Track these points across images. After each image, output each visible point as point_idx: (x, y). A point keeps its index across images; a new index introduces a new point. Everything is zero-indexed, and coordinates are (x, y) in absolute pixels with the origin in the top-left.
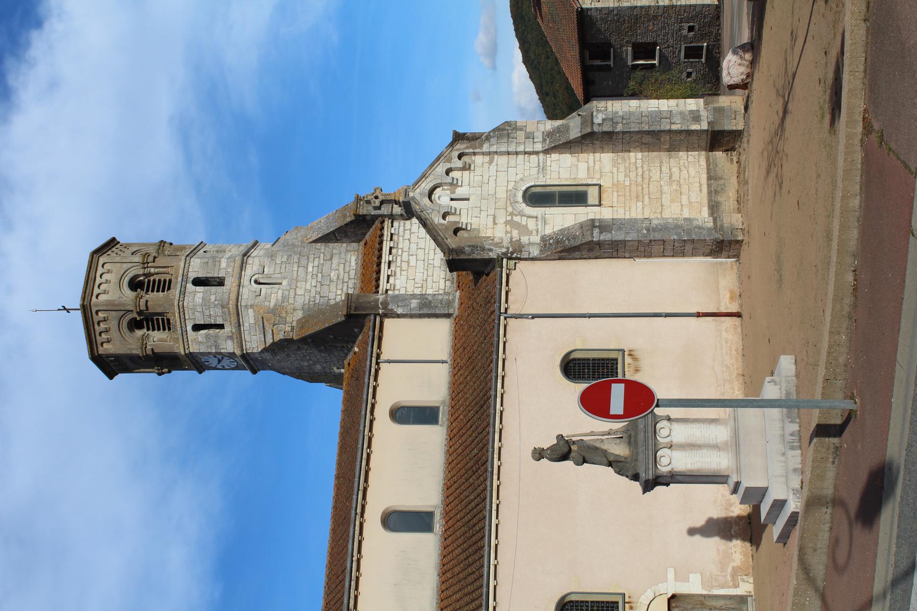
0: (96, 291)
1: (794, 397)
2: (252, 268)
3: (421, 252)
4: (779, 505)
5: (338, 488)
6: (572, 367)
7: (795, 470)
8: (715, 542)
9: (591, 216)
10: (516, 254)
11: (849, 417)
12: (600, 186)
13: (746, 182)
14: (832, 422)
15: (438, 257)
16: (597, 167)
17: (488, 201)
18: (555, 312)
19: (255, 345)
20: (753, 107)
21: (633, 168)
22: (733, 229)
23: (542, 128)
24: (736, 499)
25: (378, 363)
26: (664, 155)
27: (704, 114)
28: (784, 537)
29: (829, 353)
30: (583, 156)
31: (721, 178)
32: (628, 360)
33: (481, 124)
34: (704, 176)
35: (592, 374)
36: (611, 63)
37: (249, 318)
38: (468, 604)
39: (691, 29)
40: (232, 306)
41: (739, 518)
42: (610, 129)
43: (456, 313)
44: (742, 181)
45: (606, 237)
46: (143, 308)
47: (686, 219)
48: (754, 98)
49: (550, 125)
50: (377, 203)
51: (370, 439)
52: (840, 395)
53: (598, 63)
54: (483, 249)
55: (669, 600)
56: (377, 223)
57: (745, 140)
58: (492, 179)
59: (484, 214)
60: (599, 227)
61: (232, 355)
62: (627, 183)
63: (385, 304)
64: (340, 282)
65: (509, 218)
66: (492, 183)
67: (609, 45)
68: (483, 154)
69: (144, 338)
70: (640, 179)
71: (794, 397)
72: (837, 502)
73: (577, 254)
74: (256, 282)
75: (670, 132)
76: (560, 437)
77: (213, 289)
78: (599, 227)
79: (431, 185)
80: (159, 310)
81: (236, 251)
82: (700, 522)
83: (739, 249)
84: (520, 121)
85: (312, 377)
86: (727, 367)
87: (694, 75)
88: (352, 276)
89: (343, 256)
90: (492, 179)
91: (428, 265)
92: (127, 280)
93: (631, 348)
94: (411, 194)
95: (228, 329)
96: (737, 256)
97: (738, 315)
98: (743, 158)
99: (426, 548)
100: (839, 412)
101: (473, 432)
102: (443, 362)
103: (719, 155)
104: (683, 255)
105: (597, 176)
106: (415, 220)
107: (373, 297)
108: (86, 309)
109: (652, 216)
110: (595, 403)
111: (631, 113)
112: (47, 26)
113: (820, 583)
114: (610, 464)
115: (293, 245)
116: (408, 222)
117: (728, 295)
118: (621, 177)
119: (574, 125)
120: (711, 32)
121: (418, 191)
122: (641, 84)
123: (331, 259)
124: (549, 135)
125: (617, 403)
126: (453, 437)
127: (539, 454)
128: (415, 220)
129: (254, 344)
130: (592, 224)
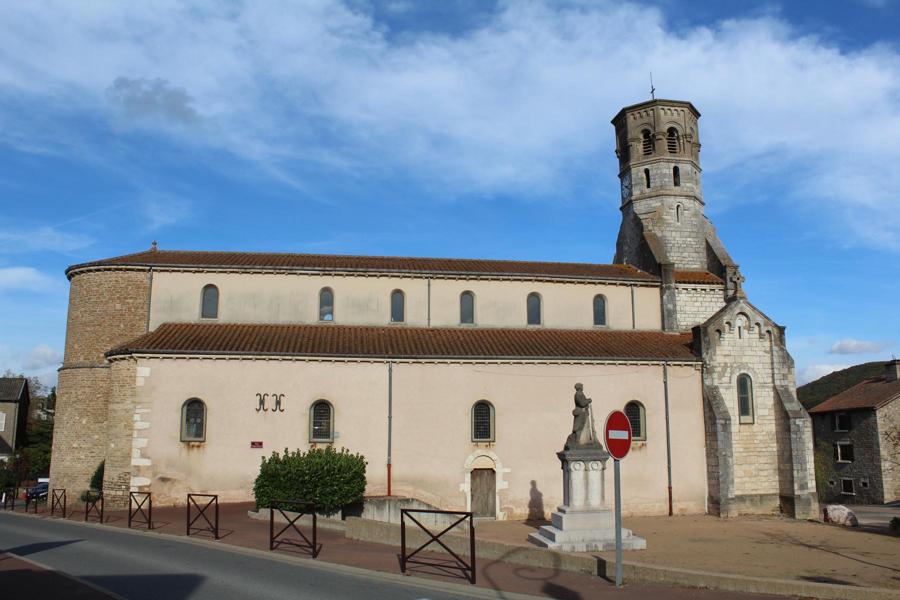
0: (666, 108)
1: (623, 548)
2: (686, 202)
4: (552, 537)
5: (552, 265)
6: (634, 407)
7: (573, 547)
8: (527, 497)
11: (611, 581)
12: (753, 424)
13: (759, 520)
14: (607, 570)
15: (701, 320)
16: (765, 422)
17: (739, 350)
18: (671, 395)
20: (812, 525)
21: (766, 445)
22: (727, 511)
23: (791, 384)
24: (555, 510)
25: (631, 285)
26: (776, 465)
27: (806, 492)
28: (532, 540)
31: (761, 503)
32: (640, 443)
33: (791, 345)
34: (762, 492)
35: (630, 418)
36: (838, 431)
37: (655, 203)
39: (865, 484)
40: (662, 192)
41: (543, 513)
44: (760, 517)
46: (657, 137)
48: (819, 526)
49: (793, 390)
50: (734, 280)
51: (583, 283)
52: (625, 576)
53: (837, 422)
54: (708, 349)
55: (492, 469)
56: (721, 280)
57: (789, 519)
58: (754, 353)
59: (731, 348)
61: (631, 194)
63: (669, 288)
67: (850, 429)
68: (771, 347)
70: (759, 450)
71: (623, 548)
72: (557, 572)
74: (678, 206)
75: (792, 470)
76: (590, 401)
80: (656, 147)
81: (697, 192)
82: (540, 488)
83: (714, 515)
84: (796, 369)
85: (619, 245)
87: (832, 486)
90: (754, 353)
91: (695, 314)
92: (674, 126)
95: (647, 190)
96: (709, 513)
97: (671, 513)
98: (776, 518)
99: (311, 316)
100: (614, 575)
102: (634, 326)
103: (777, 502)
104: (709, 478)
105: (760, 422)
106: (724, 304)
107: (673, 280)
108: (654, 102)
109: (734, 458)
110: (615, 421)
111: (804, 443)
112: (843, 57)
113: (507, 560)
114: (574, 432)
115: (703, 228)
119: (793, 406)
122: (824, 450)
124: (786, 389)
125: (616, 435)
126: (587, 334)
127: (579, 388)
128: (724, 304)
129: (639, 208)
130: (728, 419)
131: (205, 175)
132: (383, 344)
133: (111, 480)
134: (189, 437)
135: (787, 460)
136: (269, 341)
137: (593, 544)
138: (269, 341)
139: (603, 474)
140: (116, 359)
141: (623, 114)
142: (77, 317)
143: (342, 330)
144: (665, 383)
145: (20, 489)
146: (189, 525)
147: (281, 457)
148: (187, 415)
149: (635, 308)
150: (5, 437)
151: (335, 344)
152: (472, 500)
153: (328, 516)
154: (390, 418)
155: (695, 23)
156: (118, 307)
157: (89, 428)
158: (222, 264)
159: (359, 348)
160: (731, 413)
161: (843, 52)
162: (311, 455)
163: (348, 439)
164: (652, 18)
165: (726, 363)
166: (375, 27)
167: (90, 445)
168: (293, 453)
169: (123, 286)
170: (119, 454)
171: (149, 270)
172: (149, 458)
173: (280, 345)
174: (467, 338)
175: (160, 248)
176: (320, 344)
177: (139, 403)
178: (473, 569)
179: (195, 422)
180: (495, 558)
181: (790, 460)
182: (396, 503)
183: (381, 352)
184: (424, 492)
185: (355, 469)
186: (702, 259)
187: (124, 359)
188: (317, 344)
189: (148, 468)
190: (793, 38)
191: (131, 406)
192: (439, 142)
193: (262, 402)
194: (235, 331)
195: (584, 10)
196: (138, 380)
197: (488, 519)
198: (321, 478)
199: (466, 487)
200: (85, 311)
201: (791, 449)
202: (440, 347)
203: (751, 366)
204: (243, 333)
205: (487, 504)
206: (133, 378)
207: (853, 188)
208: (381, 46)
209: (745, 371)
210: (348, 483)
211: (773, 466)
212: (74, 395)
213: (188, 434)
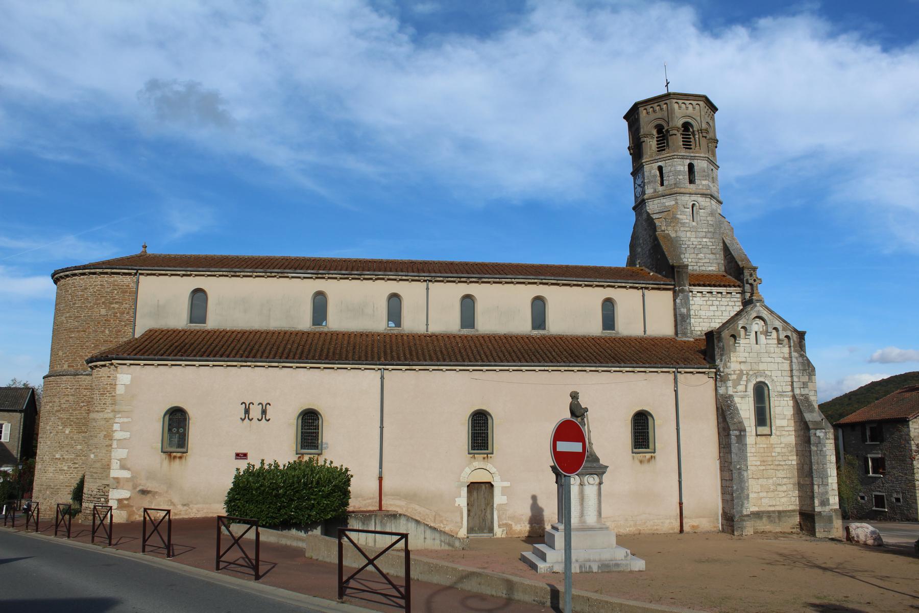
3: (719, 313)
4: (543, 557)
5: (560, 267)
8: (527, 513)
9: (747, 429)
12: (771, 435)
13: (776, 538)
15: (716, 325)
16: (784, 433)
17: (756, 356)
18: (684, 403)
20: (832, 545)
22: (742, 528)
23: (812, 393)
25: (642, 288)
26: (795, 480)
27: (827, 509)
29: (607, 602)
30: (792, 423)
31: (780, 520)
32: (648, 456)
33: (811, 353)
34: (781, 509)
36: (868, 443)
37: (669, 202)
38: (485, 353)
39: (898, 500)
42: (812, 442)
43: (678, 339)
44: (777, 536)
45: (733, 439)
46: (671, 133)
47: (748, 495)
48: (839, 546)
50: (750, 281)
51: (591, 286)
53: (868, 433)
54: (722, 355)
56: (739, 283)
57: (808, 538)
58: (772, 360)
59: (747, 355)
61: (643, 193)
62: (773, 454)
63: (682, 291)
66: (769, 360)
67: (882, 441)
68: (790, 353)
69: (651, 135)
70: (777, 463)
73: (721, 420)
74: (693, 205)
75: (812, 484)
76: (586, 410)
77: (687, 177)
80: (670, 143)
81: (714, 191)
85: (633, 247)
86: (645, 523)
87: (862, 501)
90: (772, 360)
92: (689, 120)
93: (657, 458)
94: (758, 304)
95: (660, 188)
96: (723, 531)
97: (681, 531)
98: (795, 536)
102: (645, 331)
103: (797, 519)
104: (723, 494)
105: (778, 433)
107: (687, 283)
108: (668, 96)
111: (825, 456)
112: (885, 55)
113: (459, 586)
116: (740, 304)
117: (695, 524)
118: (778, 450)
119: (814, 416)
120: (896, 514)
127: (574, 396)
128: (738, 309)
129: (652, 207)
130: (742, 430)
131: (226, 181)
132: (376, 350)
133: (90, 492)
134: (166, 447)
135: (807, 475)
136: (256, 347)
137: (587, 564)
138: (256, 347)
139: (600, 489)
140: (96, 366)
141: (635, 108)
142: (62, 323)
143: (335, 336)
144: (676, 391)
145: (23, 501)
146: (145, 541)
147: (258, 466)
148: (169, 425)
149: (646, 313)
150: (9, 448)
151: (325, 350)
152: (469, 515)
153: (306, 532)
154: (382, 428)
155: (731, 21)
156: (103, 312)
157: (72, 438)
158: (211, 267)
159: (350, 355)
160: (746, 423)
161: (885, 50)
162: (292, 467)
163: (336, 452)
164: (686, 16)
165: (741, 371)
166: (401, 29)
167: (73, 456)
168: (270, 465)
169: (108, 290)
170: (98, 465)
171: (136, 274)
172: (129, 469)
173: (267, 351)
174: (466, 344)
175: (150, 251)
176: (309, 350)
177: (119, 412)
178: (407, 596)
179: (178, 432)
180: (448, 583)
181: (810, 474)
182: (383, 518)
183: (373, 359)
184: (417, 507)
185: (339, 483)
186: (719, 261)
187: (105, 366)
188: (306, 350)
189: (127, 480)
190: (832, 36)
191: (111, 415)
192: (467, 146)
193: (247, 411)
194: (223, 337)
195: (615, 9)
196: (118, 387)
197: (485, 535)
198: (297, 492)
199: (462, 501)
200: (70, 317)
201: (811, 462)
202: (436, 354)
203: (769, 373)
204: (231, 339)
205: (484, 520)
206: (114, 386)
207: (893, 191)
208: (405, 48)
209: (762, 379)
210: (327, 496)
211: (792, 481)
212: (57, 403)
213: (170, 444)
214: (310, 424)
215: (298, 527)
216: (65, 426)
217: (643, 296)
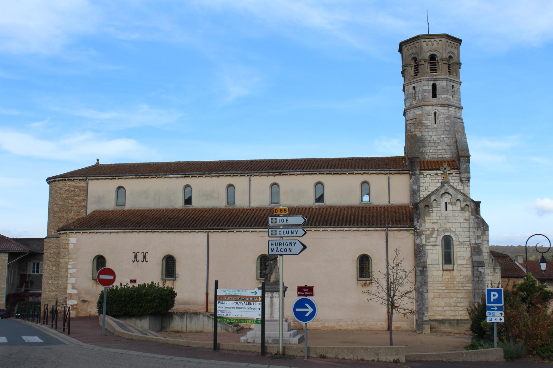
0: (427, 40)
2: (441, 109)
10: (418, 234)
12: (453, 270)
16: (463, 269)
17: (443, 218)
19: (408, 115)
25: (387, 173)
31: (458, 325)
33: (484, 213)
34: (459, 318)
37: (418, 112)
42: (475, 275)
46: (420, 63)
54: (418, 219)
58: (457, 221)
59: (438, 218)
60: (423, 270)
62: (455, 283)
63: (414, 174)
64: (436, 151)
65: (436, 229)
66: (455, 221)
70: (457, 288)
77: (431, 93)
78: (423, 270)
79: (451, 193)
88: (439, 156)
89: (449, 151)
90: (457, 221)
92: (434, 53)
95: (414, 102)
101: (354, 218)
102: (389, 202)
105: (459, 269)
107: (418, 168)
115: (455, 127)
118: (458, 280)
121: (448, 187)
123: (448, 145)
139: (283, 300)
156: (70, 201)
165: (434, 228)
171: (86, 179)
172: (76, 289)
175: (100, 163)
177: (71, 258)
189: (76, 295)
191: (67, 260)
193: (136, 257)
196: (70, 245)
209: (448, 234)
211: (468, 300)
212: (49, 254)
214: (170, 264)
215: (445, 362)
216: (53, 266)
217: (389, 178)
